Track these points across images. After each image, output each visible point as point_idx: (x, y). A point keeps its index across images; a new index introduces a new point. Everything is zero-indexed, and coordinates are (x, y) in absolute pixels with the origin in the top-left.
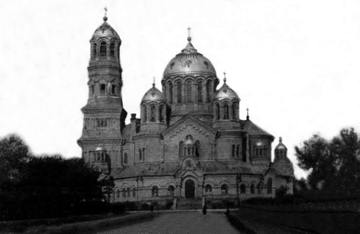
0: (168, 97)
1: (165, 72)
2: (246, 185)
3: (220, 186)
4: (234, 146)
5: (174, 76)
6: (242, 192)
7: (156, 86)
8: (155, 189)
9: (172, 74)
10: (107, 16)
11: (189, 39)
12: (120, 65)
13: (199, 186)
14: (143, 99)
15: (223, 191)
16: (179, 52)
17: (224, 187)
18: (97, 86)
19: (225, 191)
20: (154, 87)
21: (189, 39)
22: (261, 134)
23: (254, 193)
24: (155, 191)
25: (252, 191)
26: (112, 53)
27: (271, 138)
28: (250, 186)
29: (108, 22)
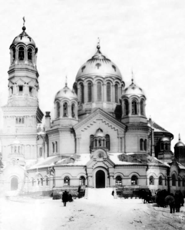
0: (35, 72)
1: (77, 76)
2: (155, 177)
3: (130, 176)
5: (84, 77)
6: (150, 184)
7: (68, 86)
8: (67, 179)
9: (84, 75)
10: (25, 26)
11: (132, 80)
12: (36, 70)
13: (91, 177)
14: (56, 97)
15: (132, 182)
16: (90, 58)
17: (134, 178)
18: (16, 89)
19: (134, 181)
20: (66, 86)
21: (132, 80)
22: (165, 132)
23: (153, 184)
24: (67, 181)
26: (30, 57)
27: (171, 136)
28: (158, 177)
29: (26, 31)
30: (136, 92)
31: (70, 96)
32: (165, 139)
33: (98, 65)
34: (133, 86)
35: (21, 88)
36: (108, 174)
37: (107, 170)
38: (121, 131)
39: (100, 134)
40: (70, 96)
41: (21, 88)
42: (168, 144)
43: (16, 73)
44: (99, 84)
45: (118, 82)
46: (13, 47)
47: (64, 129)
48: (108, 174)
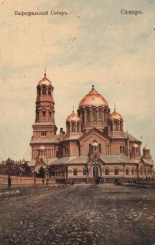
4: (121, 147)
25: (133, 174)
26: (50, 93)
27: (139, 143)
29: (94, 87)
30: (117, 117)
31: (76, 119)
32: (136, 146)
33: (93, 99)
34: (115, 113)
35: (44, 113)
36: (100, 168)
37: (100, 166)
38: (108, 142)
39: (96, 144)
40: (76, 119)
41: (44, 113)
42: (138, 149)
43: (42, 104)
44: (128, 181)
45: (106, 110)
46: (39, 88)
47: (73, 141)
48: (100, 168)
